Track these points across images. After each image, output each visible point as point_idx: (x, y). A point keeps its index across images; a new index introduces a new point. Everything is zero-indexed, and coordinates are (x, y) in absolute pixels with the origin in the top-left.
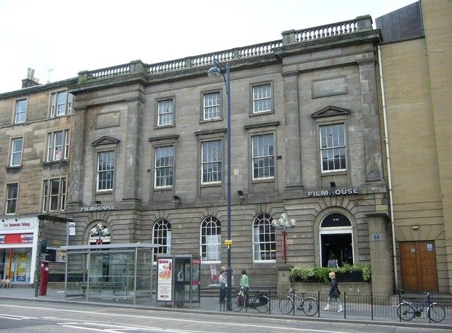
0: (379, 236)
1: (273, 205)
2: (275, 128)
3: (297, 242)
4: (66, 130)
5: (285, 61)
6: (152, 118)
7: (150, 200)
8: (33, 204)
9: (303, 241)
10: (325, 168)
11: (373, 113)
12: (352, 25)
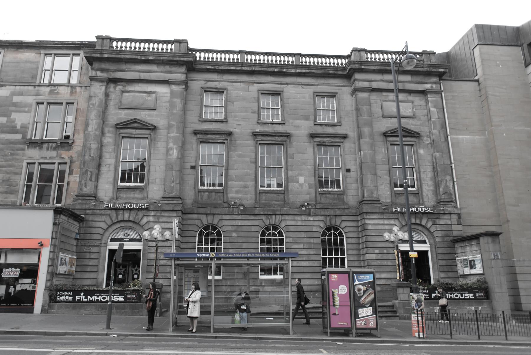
0: (497, 255)
1: (344, 218)
2: (342, 140)
3: (379, 257)
4: (68, 103)
5: (357, 76)
6: (197, 108)
7: (194, 202)
8: (6, 192)
9: (385, 257)
10: (123, 180)
11: (443, 139)
12: (169, 45)
